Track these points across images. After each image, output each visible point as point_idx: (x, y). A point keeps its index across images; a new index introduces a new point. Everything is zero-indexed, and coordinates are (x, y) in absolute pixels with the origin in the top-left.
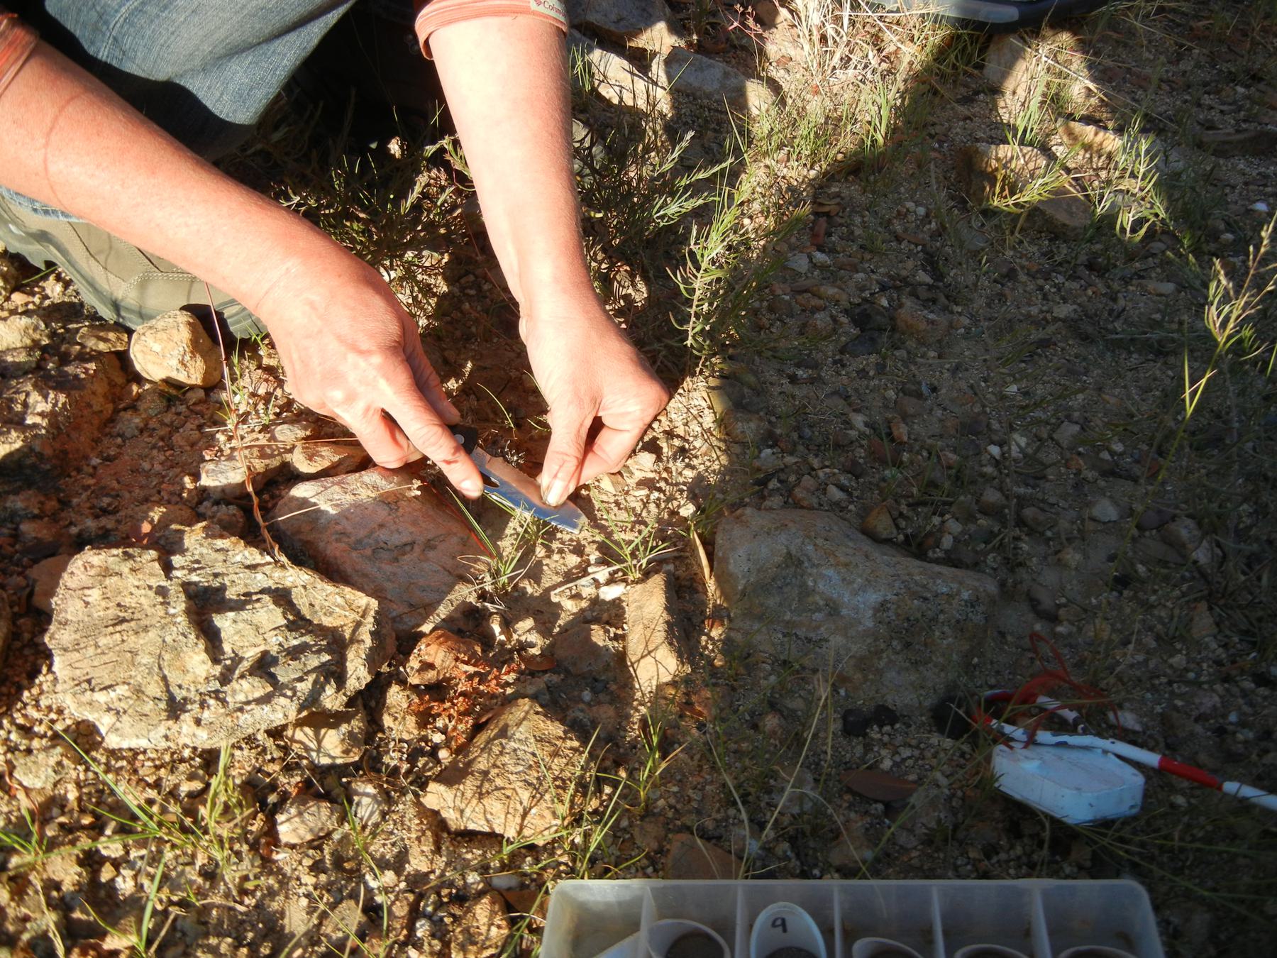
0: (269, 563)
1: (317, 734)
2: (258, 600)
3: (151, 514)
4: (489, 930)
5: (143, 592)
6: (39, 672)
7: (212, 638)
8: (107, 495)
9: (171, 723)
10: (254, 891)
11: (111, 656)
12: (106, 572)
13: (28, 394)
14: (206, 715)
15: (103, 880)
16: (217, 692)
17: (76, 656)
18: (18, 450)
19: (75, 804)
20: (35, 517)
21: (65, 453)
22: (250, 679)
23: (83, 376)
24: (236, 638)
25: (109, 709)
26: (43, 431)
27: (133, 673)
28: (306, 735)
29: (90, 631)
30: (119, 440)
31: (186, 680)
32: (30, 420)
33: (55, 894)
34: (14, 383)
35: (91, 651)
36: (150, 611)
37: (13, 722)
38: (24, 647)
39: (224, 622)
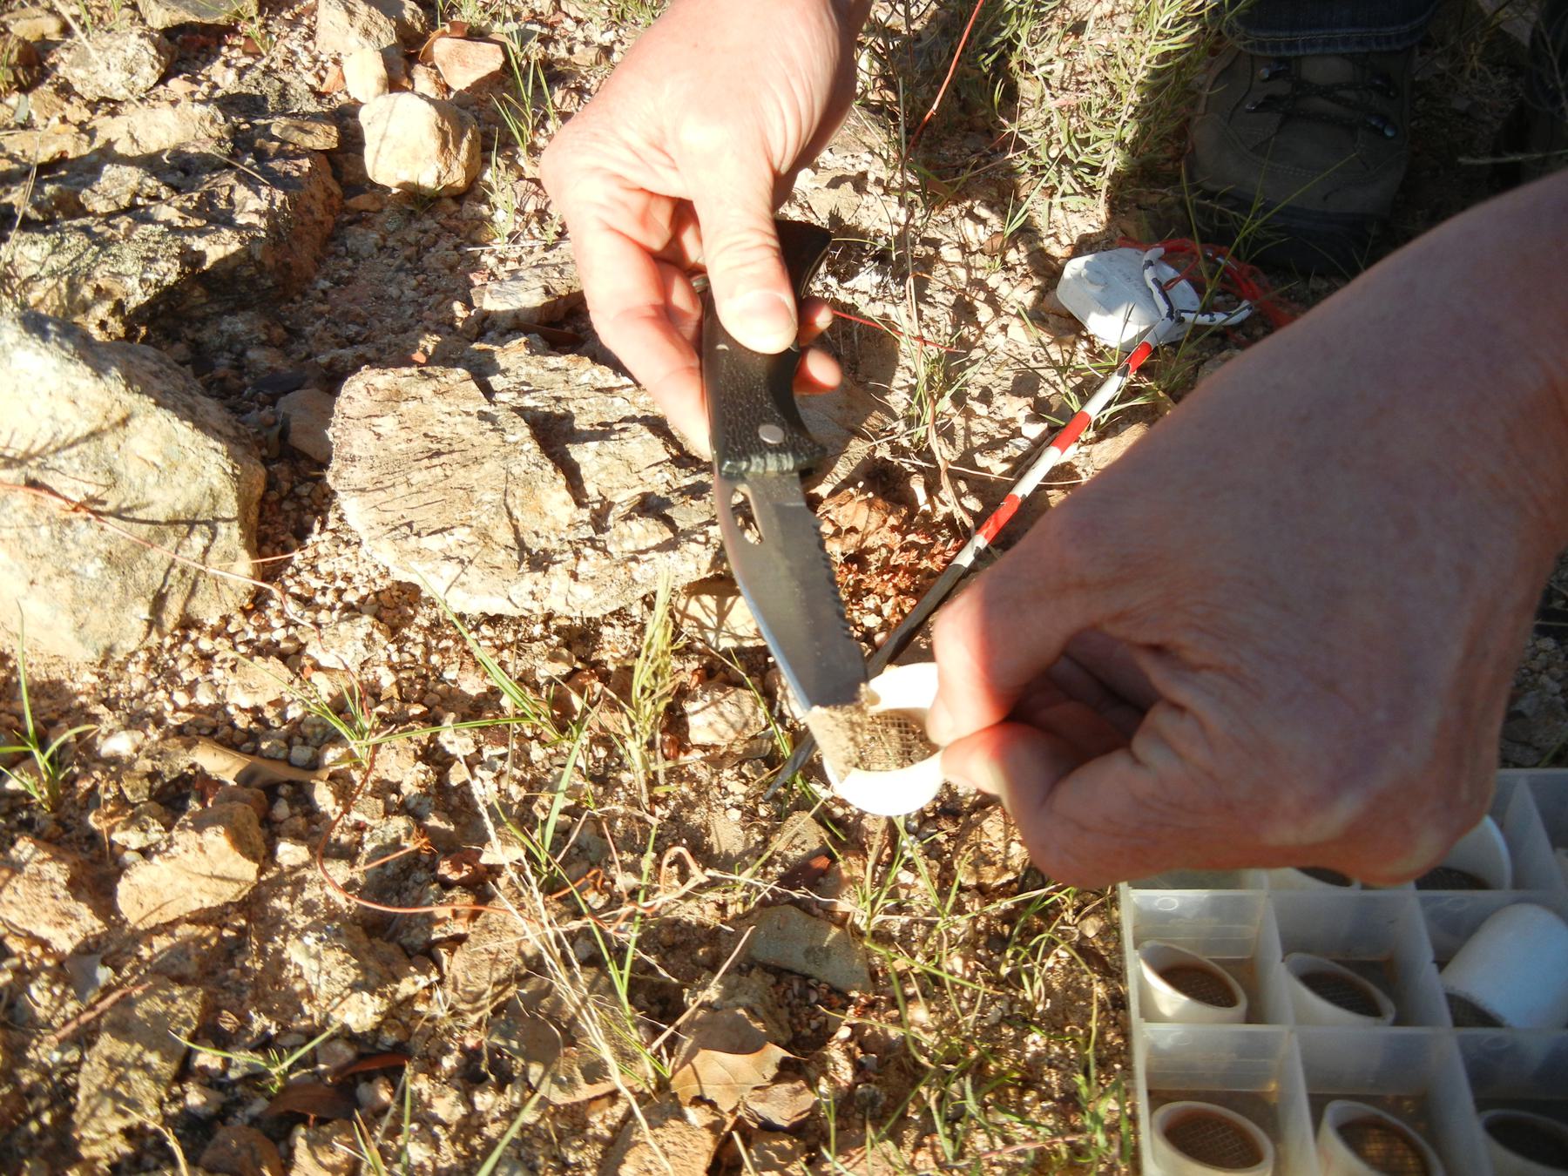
1: (720, 604)
3: (422, 342)
4: (1007, 847)
5: (459, 419)
6: (310, 530)
7: (572, 476)
8: (353, 322)
9: (539, 575)
11: (434, 495)
12: (395, 397)
13: (232, 189)
14: (583, 568)
15: (454, 783)
16: (590, 539)
17: (381, 496)
18: (234, 255)
19: (395, 692)
20: (263, 344)
21: (287, 266)
23: (296, 174)
24: (602, 475)
25: (449, 558)
26: (263, 234)
27: (474, 514)
28: (703, 607)
29: (389, 473)
30: (349, 261)
32: (241, 220)
33: (394, 797)
34: (206, 177)
35: (402, 490)
36: (477, 440)
37: (285, 590)
38: (282, 500)
39: (581, 454)
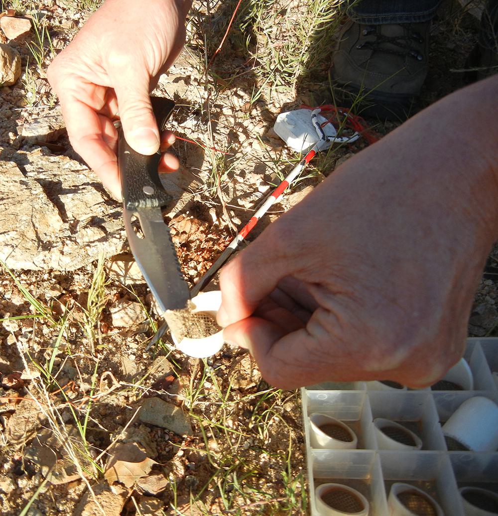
0: (86, 170)
2: (84, 189)
5: (11, 184)
10: (102, 351)
14: (66, 249)
16: (69, 237)
22: (92, 229)
25: (7, 245)
27: (18, 225)
28: (119, 266)
31: (49, 231)
36: (19, 193)
39: (65, 199)
